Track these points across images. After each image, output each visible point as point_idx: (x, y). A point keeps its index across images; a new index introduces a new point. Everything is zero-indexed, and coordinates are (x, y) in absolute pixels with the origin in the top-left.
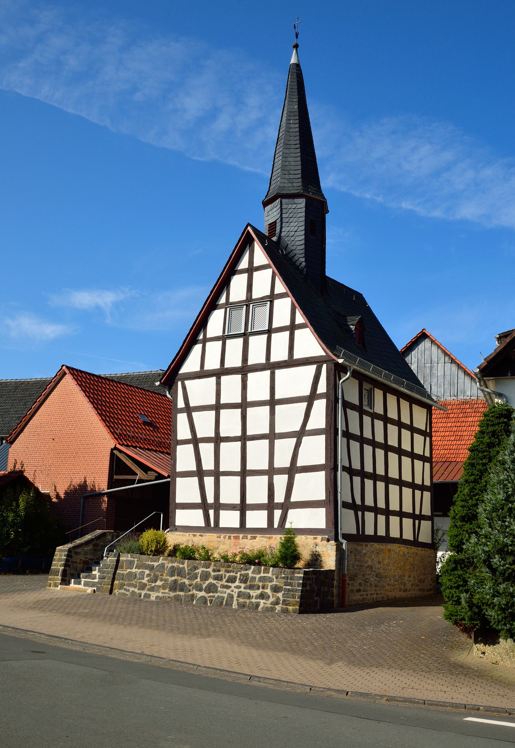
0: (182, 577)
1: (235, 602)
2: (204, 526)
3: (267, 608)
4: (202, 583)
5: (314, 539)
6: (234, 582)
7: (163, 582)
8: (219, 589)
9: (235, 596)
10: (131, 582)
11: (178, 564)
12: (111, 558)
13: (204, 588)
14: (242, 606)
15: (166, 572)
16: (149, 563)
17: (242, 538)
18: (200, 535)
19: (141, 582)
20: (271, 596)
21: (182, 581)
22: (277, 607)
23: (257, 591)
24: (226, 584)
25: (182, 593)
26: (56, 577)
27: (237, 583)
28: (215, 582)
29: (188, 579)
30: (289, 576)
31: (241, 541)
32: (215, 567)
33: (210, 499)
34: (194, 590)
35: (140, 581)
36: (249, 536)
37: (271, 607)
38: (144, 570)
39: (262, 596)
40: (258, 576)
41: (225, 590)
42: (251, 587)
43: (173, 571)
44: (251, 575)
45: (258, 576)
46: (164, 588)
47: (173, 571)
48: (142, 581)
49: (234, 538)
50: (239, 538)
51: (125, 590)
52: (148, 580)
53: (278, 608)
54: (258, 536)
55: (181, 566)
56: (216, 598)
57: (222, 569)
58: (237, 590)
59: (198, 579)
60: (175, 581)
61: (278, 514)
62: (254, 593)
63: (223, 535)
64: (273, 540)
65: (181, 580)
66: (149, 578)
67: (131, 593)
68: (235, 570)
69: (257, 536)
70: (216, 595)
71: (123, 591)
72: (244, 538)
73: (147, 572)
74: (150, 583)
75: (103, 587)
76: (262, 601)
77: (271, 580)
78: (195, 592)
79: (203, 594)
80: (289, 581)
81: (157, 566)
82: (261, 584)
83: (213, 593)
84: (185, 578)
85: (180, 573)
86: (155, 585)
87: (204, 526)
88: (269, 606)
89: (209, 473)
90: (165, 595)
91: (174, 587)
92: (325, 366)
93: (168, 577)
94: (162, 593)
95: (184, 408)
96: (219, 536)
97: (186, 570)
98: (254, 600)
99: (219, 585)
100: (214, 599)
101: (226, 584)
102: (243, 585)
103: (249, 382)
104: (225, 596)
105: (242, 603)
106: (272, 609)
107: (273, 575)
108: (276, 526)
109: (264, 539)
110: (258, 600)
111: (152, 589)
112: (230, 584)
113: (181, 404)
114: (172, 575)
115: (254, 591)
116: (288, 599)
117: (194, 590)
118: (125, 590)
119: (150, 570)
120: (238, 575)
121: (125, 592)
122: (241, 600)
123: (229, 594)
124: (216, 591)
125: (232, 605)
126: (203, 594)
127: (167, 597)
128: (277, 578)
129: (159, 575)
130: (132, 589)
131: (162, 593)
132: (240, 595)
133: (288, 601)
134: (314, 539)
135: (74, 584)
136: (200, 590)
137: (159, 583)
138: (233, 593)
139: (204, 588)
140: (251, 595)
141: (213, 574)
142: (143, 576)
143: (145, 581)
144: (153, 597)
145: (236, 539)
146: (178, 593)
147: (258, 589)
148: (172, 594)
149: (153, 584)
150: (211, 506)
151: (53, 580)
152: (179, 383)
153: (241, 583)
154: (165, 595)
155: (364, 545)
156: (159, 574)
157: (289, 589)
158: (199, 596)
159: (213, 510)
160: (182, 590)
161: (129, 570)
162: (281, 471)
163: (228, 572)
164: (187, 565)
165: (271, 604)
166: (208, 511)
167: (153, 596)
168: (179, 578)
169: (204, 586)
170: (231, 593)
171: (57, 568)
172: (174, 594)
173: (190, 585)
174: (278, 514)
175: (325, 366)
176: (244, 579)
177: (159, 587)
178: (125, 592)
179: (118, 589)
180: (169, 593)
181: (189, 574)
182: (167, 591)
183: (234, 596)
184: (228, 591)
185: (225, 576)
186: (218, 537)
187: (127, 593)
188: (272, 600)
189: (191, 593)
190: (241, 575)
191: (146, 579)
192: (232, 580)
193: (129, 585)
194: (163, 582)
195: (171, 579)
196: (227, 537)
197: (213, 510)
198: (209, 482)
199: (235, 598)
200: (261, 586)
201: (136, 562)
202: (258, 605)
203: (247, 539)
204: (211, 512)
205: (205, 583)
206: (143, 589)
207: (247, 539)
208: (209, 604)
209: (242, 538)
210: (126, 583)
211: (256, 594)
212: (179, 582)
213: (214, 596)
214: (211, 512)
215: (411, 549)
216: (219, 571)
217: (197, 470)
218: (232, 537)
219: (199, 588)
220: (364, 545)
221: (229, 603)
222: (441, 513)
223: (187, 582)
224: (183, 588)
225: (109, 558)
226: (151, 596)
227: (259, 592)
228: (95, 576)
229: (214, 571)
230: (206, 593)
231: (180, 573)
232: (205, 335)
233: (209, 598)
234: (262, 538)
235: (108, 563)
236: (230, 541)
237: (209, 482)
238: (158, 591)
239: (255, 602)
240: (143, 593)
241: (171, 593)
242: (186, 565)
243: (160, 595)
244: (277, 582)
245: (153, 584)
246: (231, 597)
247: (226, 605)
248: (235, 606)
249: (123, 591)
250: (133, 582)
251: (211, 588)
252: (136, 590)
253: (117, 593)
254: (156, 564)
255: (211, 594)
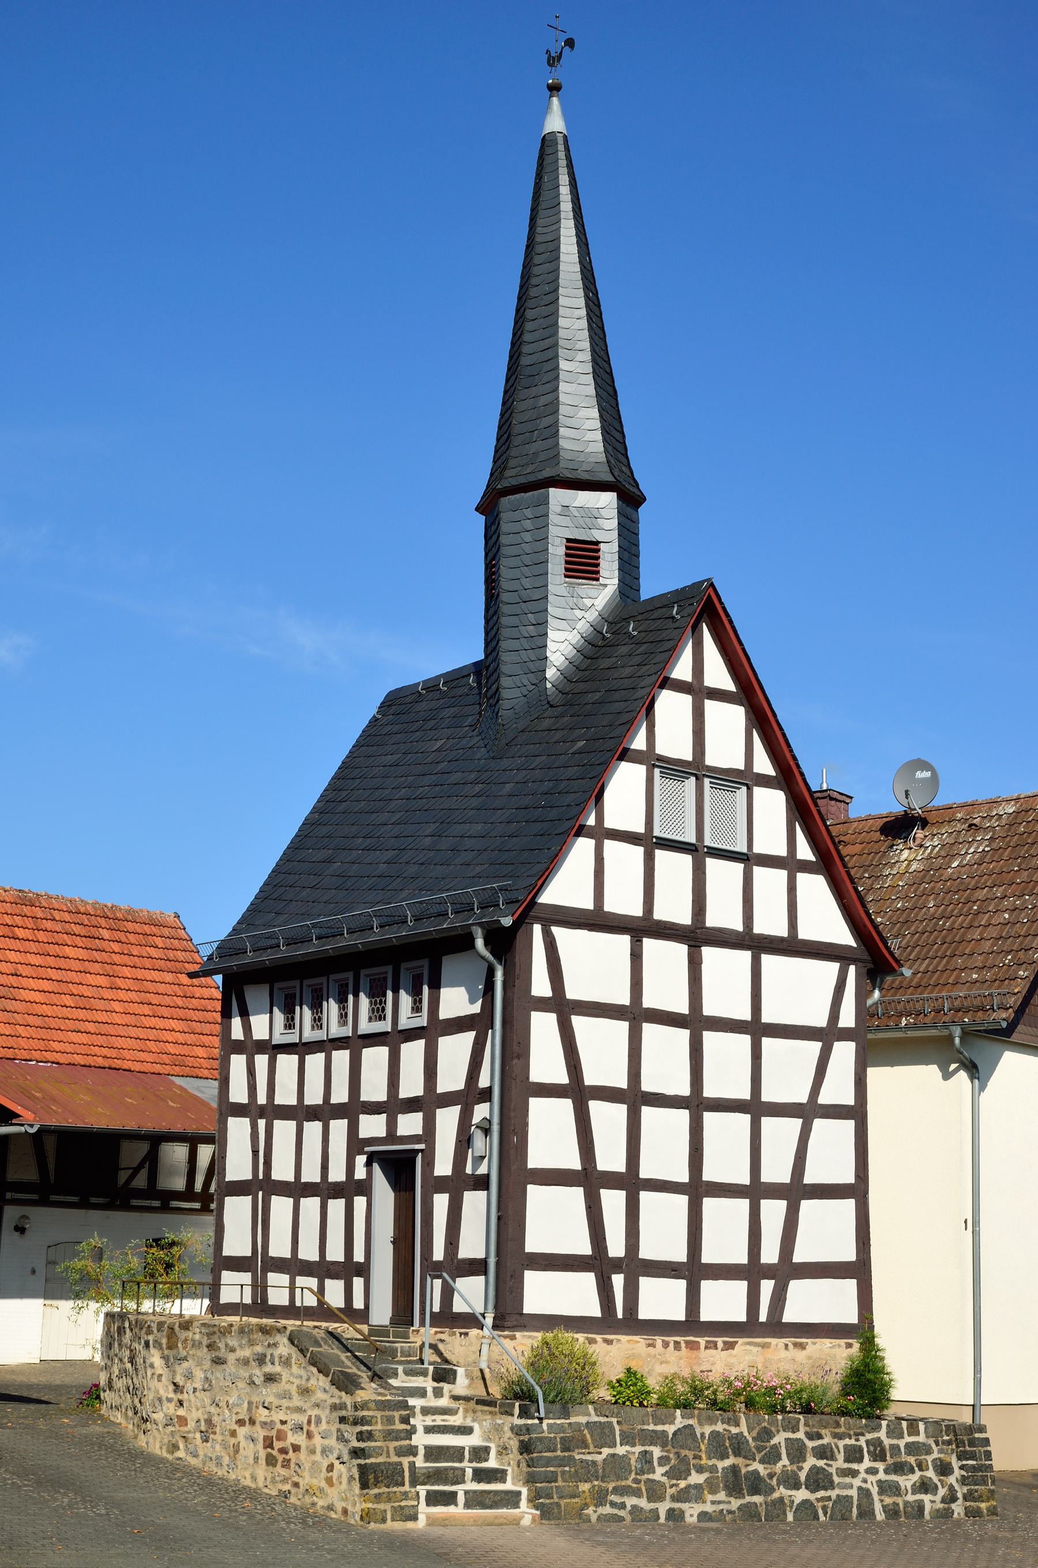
0: (745, 1457)
1: (878, 1507)
2: (599, 1315)
3: (938, 1511)
4: (795, 1468)
5: (847, 1348)
6: (860, 1460)
7: (706, 1475)
8: (836, 1479)
9: (875, 1490)
10: (623, 1483)
11: (725, 1426)
12: (551, 1421)
13: (803, 1478)
14: (892, 1512)
15: (703, 1447)
16: (651, 1427)
17: (706, 1348)
18: (607, 1341)
19: (648, 1479)
20: (939, 1484)
21: (750, 1468)
22: (953, 1506)
23: (910, 1476)
24: (846, 1465)
25: (757, 1499)
26: (395, 1489)
27: (867, 1463)
28: (821, 1463)
29: (762, 1462)
30: (965, 1438)
31: (704, 1354)
32: (808, 1428)
33: (616, 1248)
34: (781, 1487)
35: (646, 1476)
36: (720, 1341)
37: (945, 1509)
38: (647, 1448)
39: (925, 1486)
40: (902, 1443)
41: (848, 1480)
42: (899, 1468)
43: (719, 1446)
44: (887, 1442)
45: (902, 1443)
46: (713, 1491)
47: (719, 1446)
48: (651, 1476)
49: (686, 1347)
50: (698, 1348)
51: (613, 1504)
52: (667, 1472)
53: (958, 1509)
54: (741, 1341)
55: (734, 1430)
56: (835, 1502)
57: (823, 1432)
58: (872, 1478)
59: (785, 1461)
60: (734, 1469)
61: (767, 1287)
62: (907, 1482)
63: (659, 1340)
64: (770, 1350)
65: (747, 1465)
66: (667, 1468)
67: (631, 1513)
68: (852, 1433)
69: (738, 1342)
70: (833, 1494)
71: (607, 1510)
72: (710, 1348)
73: (657, 1452)
74: (674, 1482)
75: (558, 1505)
76: (926, 1498)
77: (929, 1451)
78: (783, 1491)
79: (801, 1495)
80: (968, 1448)
81: (675, 1434)
82: (912, 1460)
83: (826, 1489)
84: (754, 1460)
85: (739, 1446)
86: (689, 1486)
87: (599, 1315)
88: (941, 1506)
89: (612, 1180)
90: (721, 1507)
91: (735, 1481)
92: (852, 969)
93: (714, 1461)
94: (713, 1503)
95: (549, 998)
96: (651, 1342)
97: (750, 1440)
98: (910, 1498)
99: (833, 1470)
100: (831, 1504)
101: (846, 1465)
102: (881, 1466)
103: (705, 968)
104: (853, 1493)
105: (891, 1507)
106: (947, 1514)
107: (927, 1437)
108: (763, 1317)
109: (751, 1348)
110: (919, 1497)
111: (682, 1496)
112: (855, 1466)
113: (541, 986)
114: (723, 1456)
115: (904, 1477)
116: (976, 1487)
117: (781, 1487)
118: (613, 1504)
119: (663, 1447)
120: (862, 1442)
121: (615, 1511)
122: (888, 1500)
123: (860, 1488)
124: (830, 1485)
125: (873, 1514)
126: (801, 1495)
127: (725, 1512)
128: (937, 1443)
129: (691, 1457)
130: (631, 1501)
131: (713, 1503)
132: (884, 1488)
133: (976, 1491)
134: (847, 1348)
135: (428, 1505)
136: (797, 1486)
137: (696, 1478)
138: (869, 1486)
139: (803, 1478)
140: (903, 1488)
141: (810, 1444)
142: (650, 1462)
143: (659, 1474)
144: (691, 1516)
145: (691, 1349)
146: (748, 1499)
147: (912, 1471)
148: (735, 1504)
149: (683, 1484)
150: (617, 1265)
151: (389, 1500)
152: (537, 929)
153: (875, 1460)
154: (721, 1507)
155: (720, 1345)
156: (690, 1454)
157: (973, 1466)
158: (797, 1501)
159: (622, 1276)
160: (755, 1491)
161: (606, 1451)
162: (775, 1191)
163: (840, 1439)
164: (747, 1426)
165: (943, 1501)
166: (610, 1278)
167: (692, 1512)
168: (740, 1461)
169: (803, 1476)
170: (864, 1485)
171: (388, 1460)
172: (735, 1504)
173: (771, 1476)
174: (767, 1287)
175: (852, 969)
176: (878, 1453)
177: (698, 1487)
178: (615, 1511)
179: (596, 1506)
180: (730, 1502)
181: (759, 1449)
182: (722, 1496)
183: (873, 1493)
184: (857, 1482)
185: (837, 1447)
186: (649, 1345)
187: (622, 1513)
188: (942, 1492)
189: (776, 1495)
190: (867, 1442)
191: (660, 1470)
192: (854, 1455)
193: (618, 1491)
194: (706, 1475)
195: (722, 1464)
196: (672, 1345)
197: (622, 1276)
198: (613, 1201)
199: (876, 1497)
200: (914, 1465)
201: (617, 1428)
202: (920, 1507)
203: (716, 1348)
204: (618, 1281)
205: (801, 1469)
206: (661, 1499)
207: (716, 1348)
208: (822, 1518)
209: (706, 1348)
210: (611, 1486)
211: (912, 1482)
212: (743, 1471)
213: (829, 1498)
214: (618, 1281)
215: (802, 1347)
216: (820, 1437)
217: (584, 1169)
218: (683, 1345)
219: (791, 1481)
220: (720, 1345)
221: (866, 1513)
222: (35, 1197)
223: (762, 1469)
224: (757, 1485)
225: (545, 1422)
226: (687, 1515)
227: (915, 1477)
228: (460, 1473)
229: (810, 1436)
230: (812, 1492)
231: (739, 1446)
232: (600, 818)
233: (820, 1504)
234: (748, 1347)
235: (546, 1434)
236: (677, 1353)
237: (613, 1201)
238: (700, 1499)
239: (915, 1501)
240: (663, 1508)
241: (732, 1499)
242: (744, 1428)
243: (709, 1508)
244: (941, 1453)
245: (683, 1484)
246: (865, 1493)
247: (860, 1515)
248: (880, 1516)
249: (607, 1510)
250: (629, 1482)
251: (819, 1480)
252: (643, 1503)
253: (594, 1518)
254: (671, 1429)
255: (822, 1494)
